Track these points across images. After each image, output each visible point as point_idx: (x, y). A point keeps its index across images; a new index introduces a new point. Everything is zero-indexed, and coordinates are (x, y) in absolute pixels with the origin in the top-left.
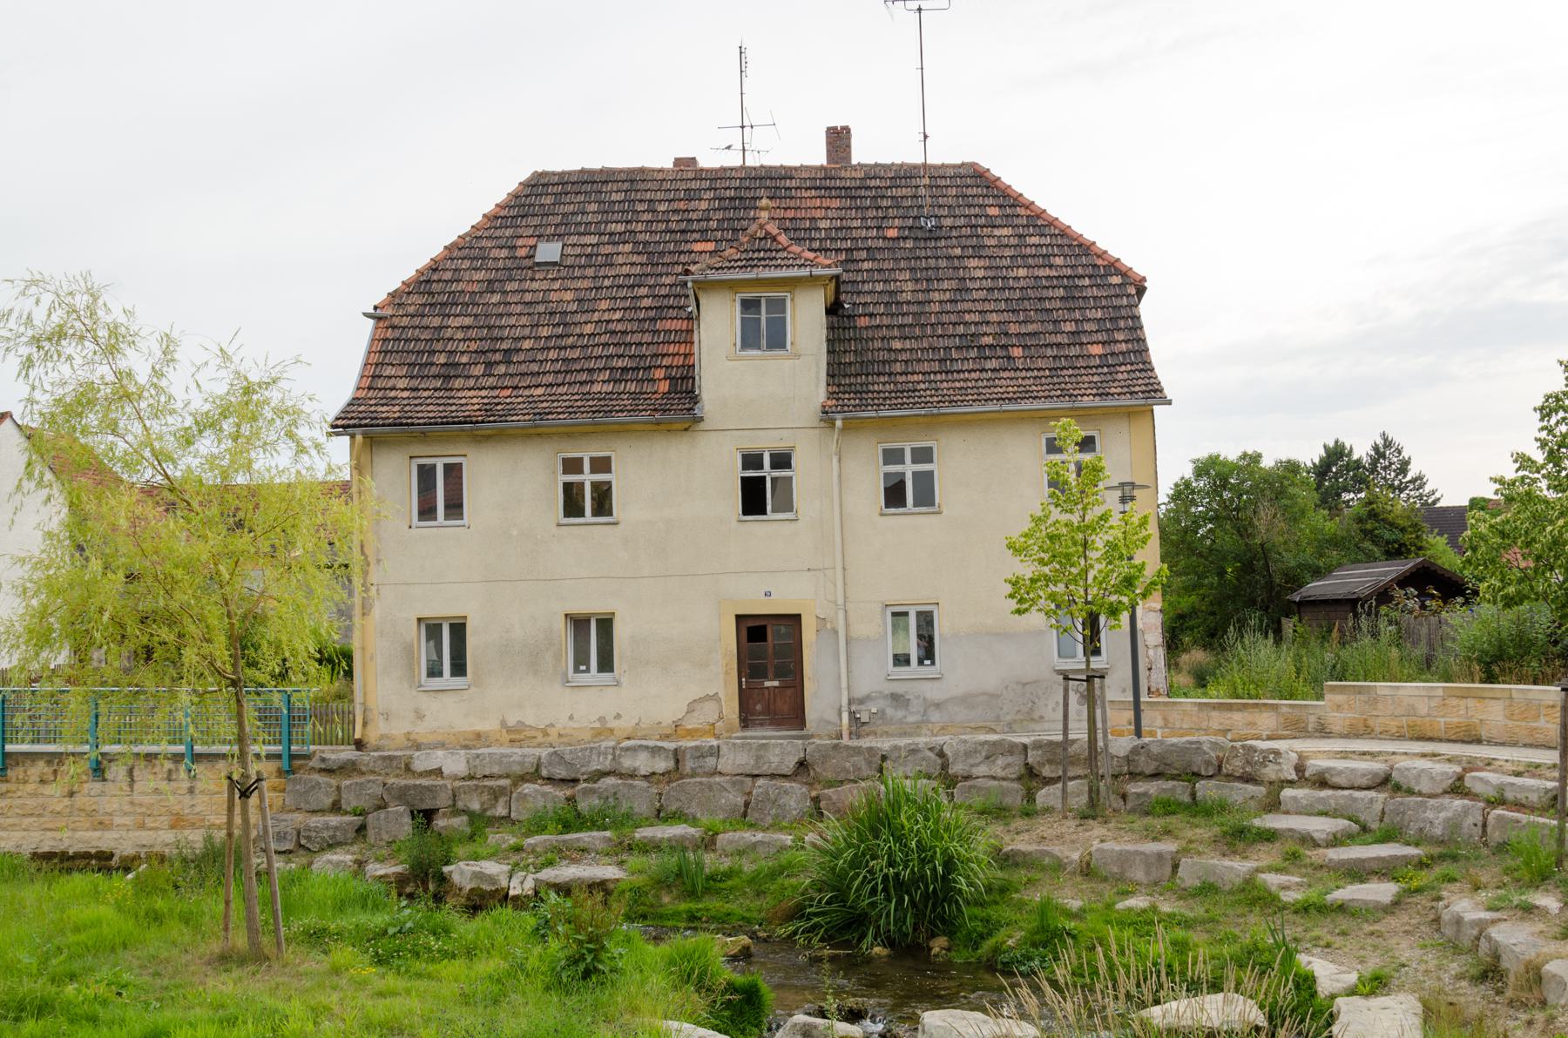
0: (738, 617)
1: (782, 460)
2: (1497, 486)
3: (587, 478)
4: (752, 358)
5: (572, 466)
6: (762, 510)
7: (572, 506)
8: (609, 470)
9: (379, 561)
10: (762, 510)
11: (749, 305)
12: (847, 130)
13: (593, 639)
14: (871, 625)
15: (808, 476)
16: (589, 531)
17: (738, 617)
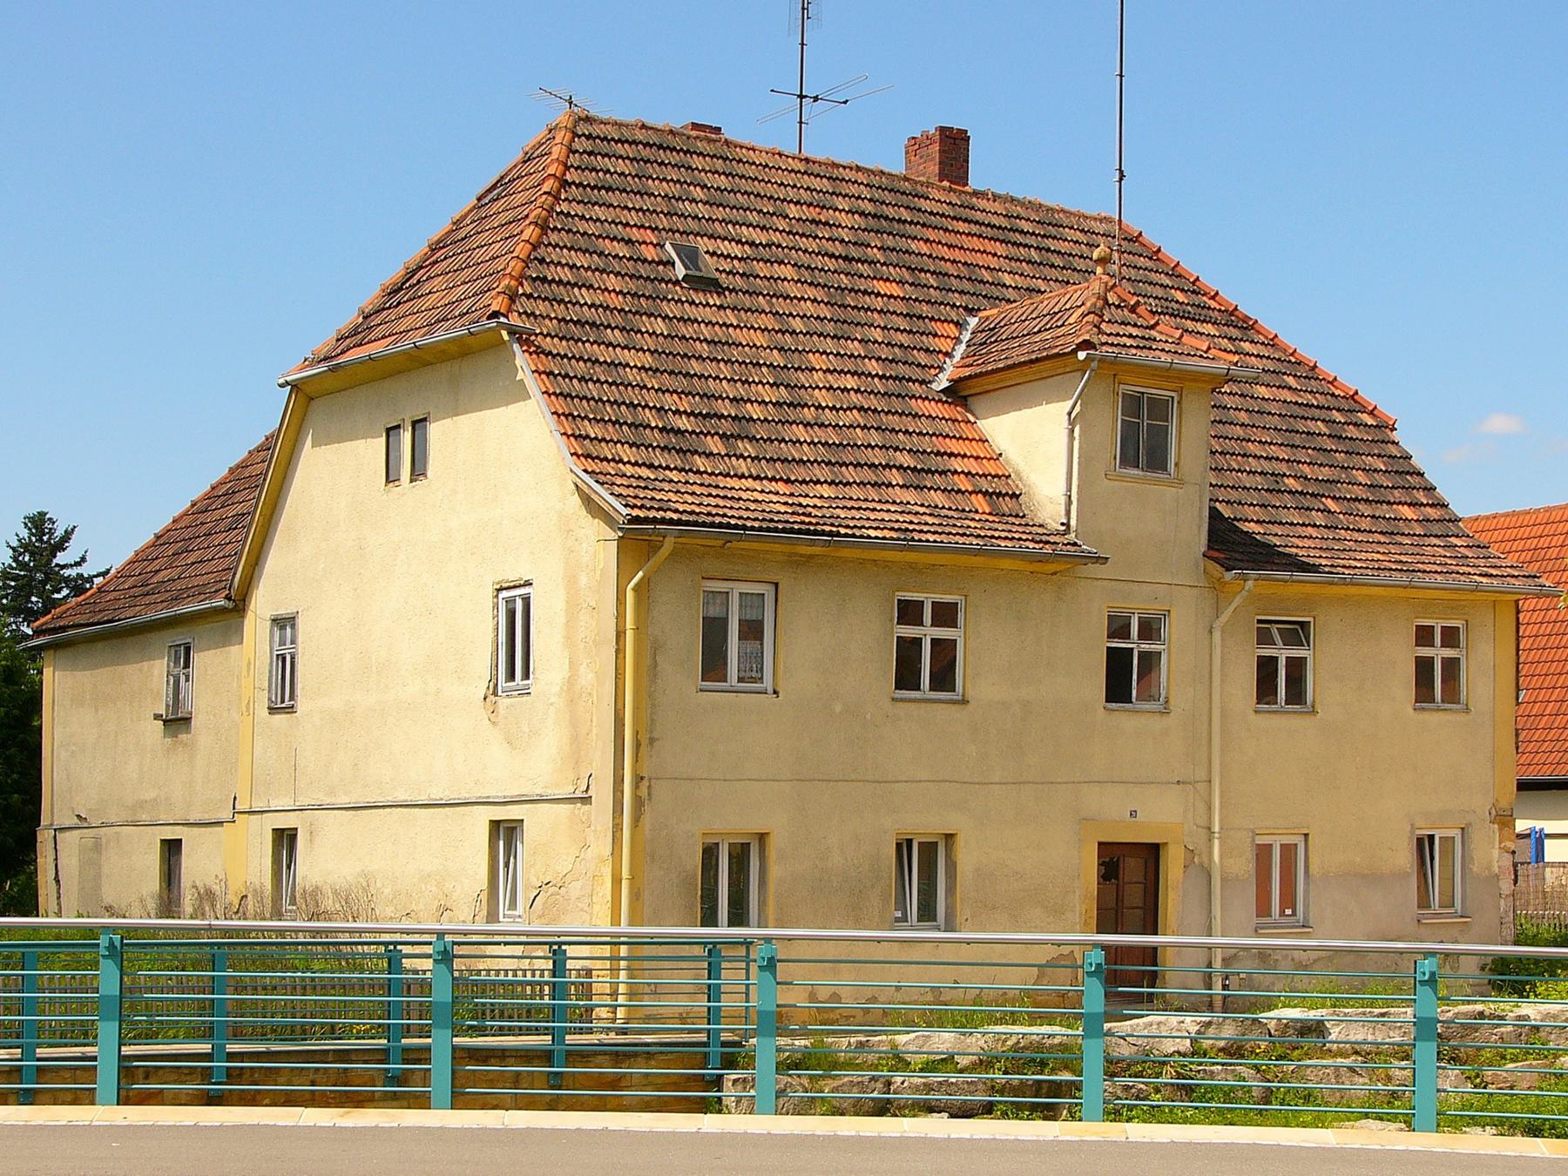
0: (1100, 844)
1: (1149, 629)
2: (59, 533)
3: (928, 632)
4: (1135, 479)
5: (909, 612)
6: (1127, 699)
7: (906, 677)
8: (953, 624)
9: (652, 741)
10: (1127, 699)
11: (1133, 404)
12: (42, 514)
13: (922, 870)
14: (1229, 859)
15: (1178, 653)
16: (926, 713)
17: (1100, 844)
